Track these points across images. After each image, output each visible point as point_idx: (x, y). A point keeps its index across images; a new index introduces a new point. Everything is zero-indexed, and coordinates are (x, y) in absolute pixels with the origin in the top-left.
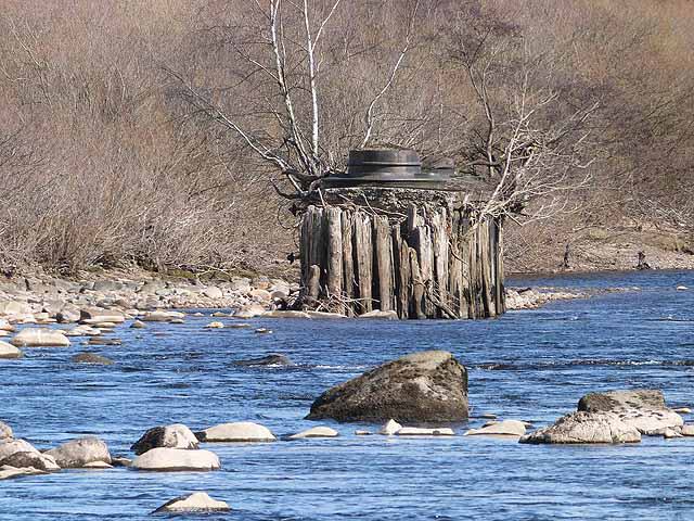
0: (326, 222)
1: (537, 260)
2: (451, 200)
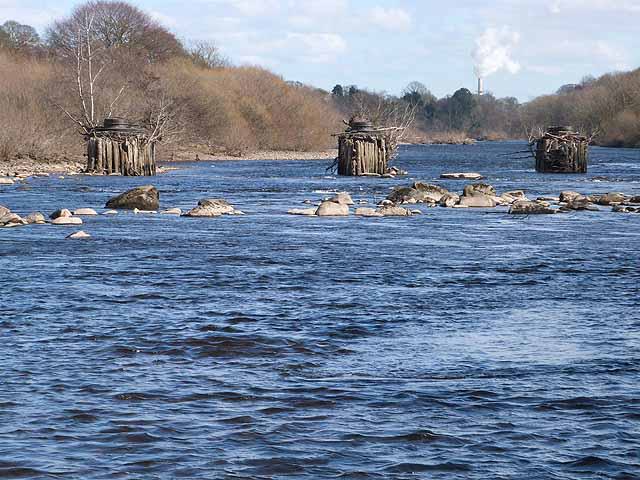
0: (97, 143)
1: (163, 157)
2: (138, 136)
